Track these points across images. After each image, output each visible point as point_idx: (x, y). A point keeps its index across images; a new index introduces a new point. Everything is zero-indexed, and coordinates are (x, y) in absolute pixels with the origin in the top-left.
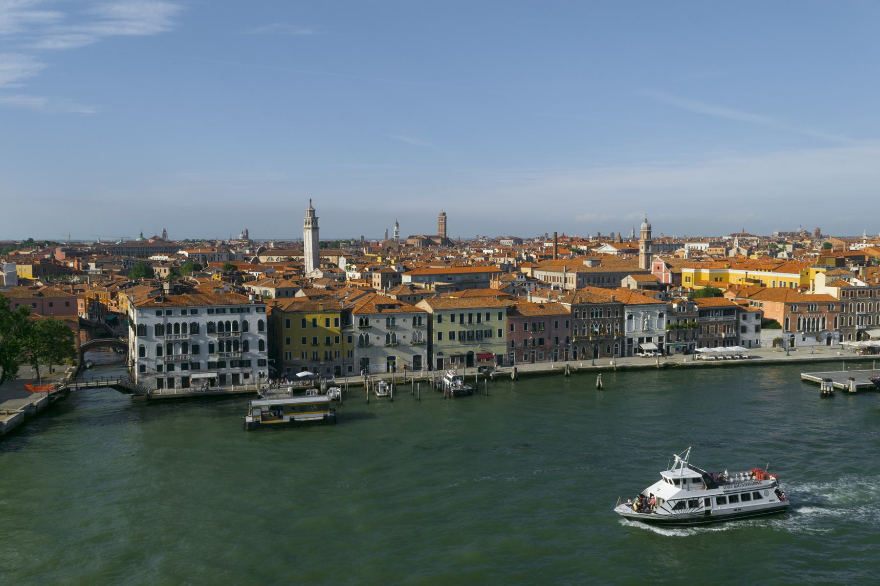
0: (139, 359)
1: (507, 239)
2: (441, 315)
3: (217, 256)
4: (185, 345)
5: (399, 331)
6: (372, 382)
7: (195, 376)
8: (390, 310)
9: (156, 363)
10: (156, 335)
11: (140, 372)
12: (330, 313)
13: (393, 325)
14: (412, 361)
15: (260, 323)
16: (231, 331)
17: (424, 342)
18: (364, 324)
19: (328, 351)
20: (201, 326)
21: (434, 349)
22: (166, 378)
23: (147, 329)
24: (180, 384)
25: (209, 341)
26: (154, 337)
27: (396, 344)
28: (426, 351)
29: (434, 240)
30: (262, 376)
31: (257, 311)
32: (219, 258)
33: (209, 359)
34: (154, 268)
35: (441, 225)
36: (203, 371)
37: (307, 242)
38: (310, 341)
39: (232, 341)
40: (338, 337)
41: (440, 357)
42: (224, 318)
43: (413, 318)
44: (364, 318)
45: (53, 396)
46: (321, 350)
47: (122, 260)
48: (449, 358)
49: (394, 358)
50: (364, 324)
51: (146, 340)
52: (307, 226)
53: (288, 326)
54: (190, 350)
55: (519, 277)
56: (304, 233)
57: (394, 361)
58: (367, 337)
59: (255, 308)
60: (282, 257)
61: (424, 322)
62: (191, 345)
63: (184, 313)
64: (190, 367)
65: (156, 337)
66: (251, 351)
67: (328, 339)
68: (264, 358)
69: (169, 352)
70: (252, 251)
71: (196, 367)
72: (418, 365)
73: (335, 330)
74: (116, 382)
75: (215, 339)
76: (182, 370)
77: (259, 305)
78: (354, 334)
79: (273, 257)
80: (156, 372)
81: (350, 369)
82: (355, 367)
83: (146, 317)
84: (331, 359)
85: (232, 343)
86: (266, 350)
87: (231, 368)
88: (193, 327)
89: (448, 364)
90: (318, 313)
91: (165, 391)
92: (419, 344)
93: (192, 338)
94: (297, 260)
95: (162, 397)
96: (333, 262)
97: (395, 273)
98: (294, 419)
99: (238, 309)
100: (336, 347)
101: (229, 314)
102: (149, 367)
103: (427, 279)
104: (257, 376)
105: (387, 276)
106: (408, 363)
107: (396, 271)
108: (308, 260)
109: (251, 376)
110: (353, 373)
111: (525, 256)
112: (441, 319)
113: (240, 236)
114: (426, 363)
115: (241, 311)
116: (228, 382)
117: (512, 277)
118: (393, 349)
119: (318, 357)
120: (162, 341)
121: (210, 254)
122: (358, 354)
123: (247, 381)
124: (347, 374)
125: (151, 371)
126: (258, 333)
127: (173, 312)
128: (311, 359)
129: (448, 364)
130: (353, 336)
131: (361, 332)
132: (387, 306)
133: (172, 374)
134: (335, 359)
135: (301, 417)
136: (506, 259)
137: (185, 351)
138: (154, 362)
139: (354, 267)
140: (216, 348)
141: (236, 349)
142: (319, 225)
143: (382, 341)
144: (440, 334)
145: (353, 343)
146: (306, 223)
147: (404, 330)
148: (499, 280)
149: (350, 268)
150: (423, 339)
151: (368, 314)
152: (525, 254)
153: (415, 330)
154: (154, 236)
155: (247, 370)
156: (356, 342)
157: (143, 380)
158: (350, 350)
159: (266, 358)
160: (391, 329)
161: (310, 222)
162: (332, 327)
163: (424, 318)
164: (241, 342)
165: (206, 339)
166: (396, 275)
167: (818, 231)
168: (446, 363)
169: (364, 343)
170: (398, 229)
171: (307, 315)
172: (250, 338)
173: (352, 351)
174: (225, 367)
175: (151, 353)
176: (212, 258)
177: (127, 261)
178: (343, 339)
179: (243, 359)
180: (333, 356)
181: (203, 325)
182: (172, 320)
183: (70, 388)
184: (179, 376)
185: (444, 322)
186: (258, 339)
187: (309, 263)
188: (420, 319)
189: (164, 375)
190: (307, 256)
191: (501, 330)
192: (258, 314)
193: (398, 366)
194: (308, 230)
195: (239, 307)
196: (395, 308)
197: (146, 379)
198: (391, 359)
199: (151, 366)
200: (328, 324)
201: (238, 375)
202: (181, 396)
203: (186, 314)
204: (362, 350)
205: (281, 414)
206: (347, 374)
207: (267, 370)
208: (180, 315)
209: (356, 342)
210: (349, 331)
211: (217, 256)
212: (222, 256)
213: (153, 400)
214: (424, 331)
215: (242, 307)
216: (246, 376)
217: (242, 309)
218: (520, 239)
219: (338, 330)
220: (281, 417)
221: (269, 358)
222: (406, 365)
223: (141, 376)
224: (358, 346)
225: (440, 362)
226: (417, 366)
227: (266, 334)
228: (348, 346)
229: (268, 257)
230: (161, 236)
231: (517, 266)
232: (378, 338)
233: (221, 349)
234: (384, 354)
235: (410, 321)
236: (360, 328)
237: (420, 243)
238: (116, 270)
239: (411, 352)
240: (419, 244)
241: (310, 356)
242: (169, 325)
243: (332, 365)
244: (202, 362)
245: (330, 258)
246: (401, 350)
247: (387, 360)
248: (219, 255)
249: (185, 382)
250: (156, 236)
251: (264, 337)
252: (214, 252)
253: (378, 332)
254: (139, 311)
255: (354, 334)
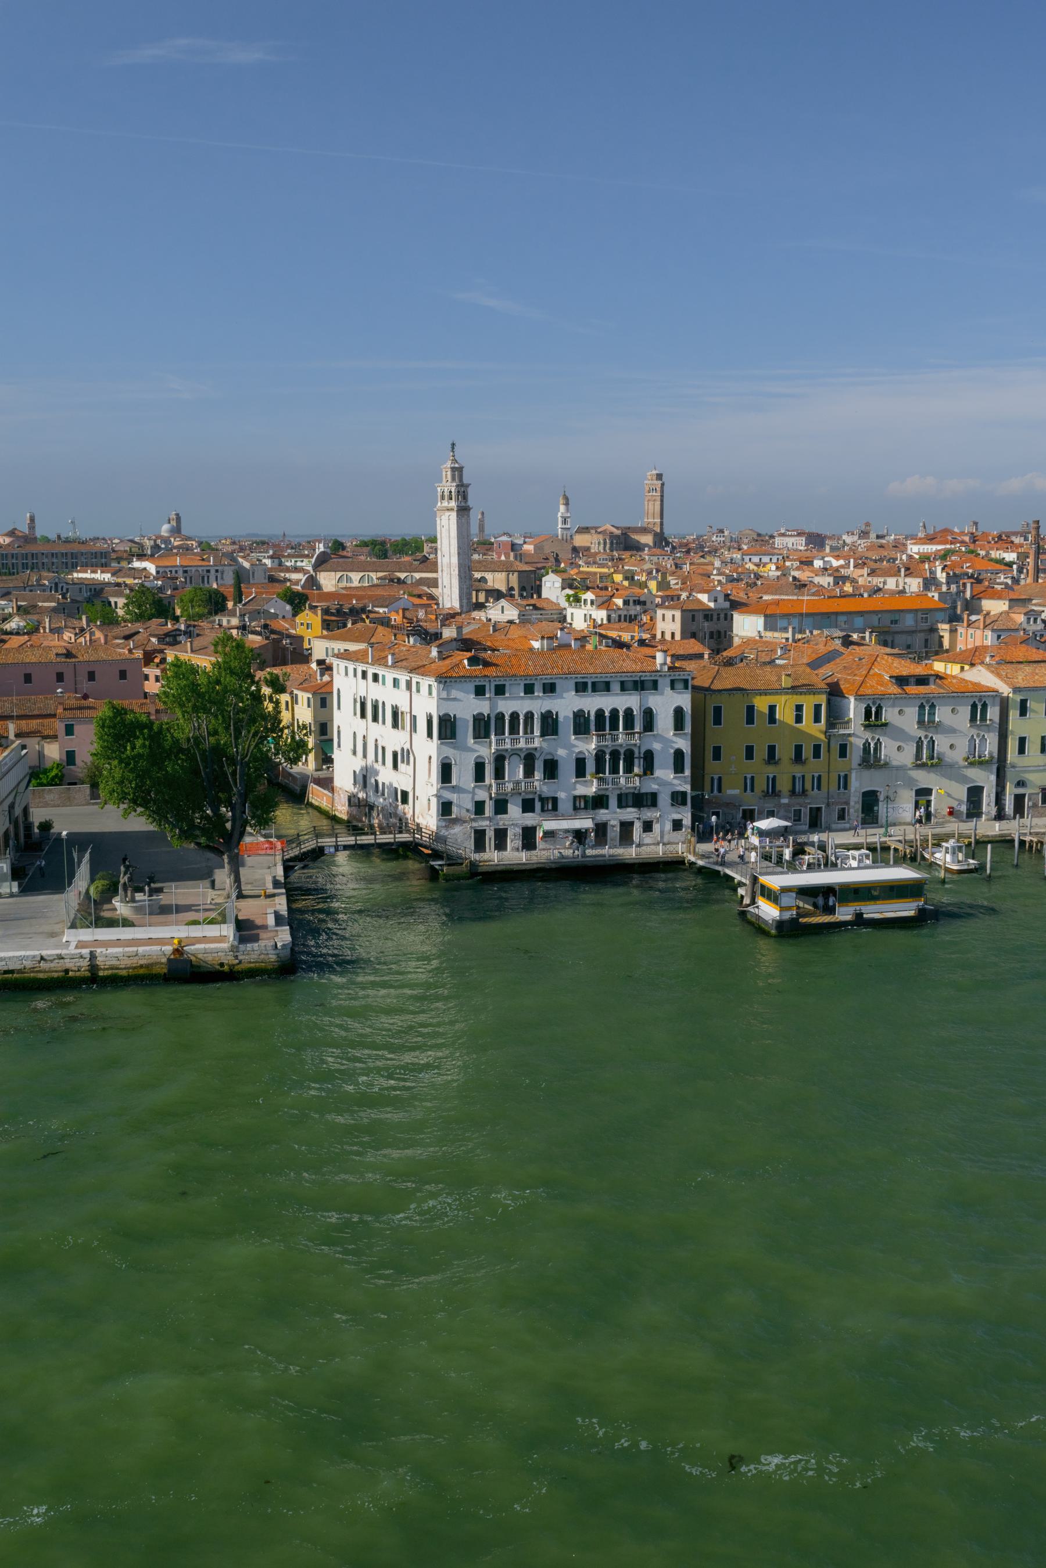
0: (442, 788)
1: (791, 536)
2: (1026, 700)
3: (213, 572)
4: (529, 760)
5: (942, 733)
6: (916, 840)
7: (550, 825)
8: (922, 689)
9: (473, 798)
10: (475, 738)
11: (443, 815)
12: (805, 694)
13: (932, 721)
14: (965, 800)
15: (679, 712)
16: (621, 729)
17: (992, 757)
18: (873, 718)
19: (798, 775)
20: (561, 719)
21: (1010, 773)
22: (492, 828)
23: (458, 723)
24: (519, 843)
25: (577, 750)
26: (471, 741)
27: (933, 763)
28: (993, 778)
29: (636, 537)
30: (677, 825)
31: (673, 688)
32: (217, 577)
33: (575, 789)
34: (112, 600)
35: (651, 503)
36: (563, 815)
37: (445, 542)
38: (761, 753)
39: (622, 751)
40: (820, 746)
41: (1020, 791)
42: (606, 702)
43: (972, 706)
44: (874, 703)
45: (291, 864)
46: (785, 772)
47: (46, 582)
48: (1038, 794)
49: (928, 792)
50: (873, 718)
51: (454, 748)
52: (445, 504)
53: (717, 721)
54: (539, 771)
55: (1029, 619)
56: (438, 519)
57: (928, 798)
58: (878, 743)
59: (668, 681)
60: (373, 575)
61: (993, 713)
62: (542, 758)
63: (529, 689)
64: (538, 805)
65: (475, 743)
66: (658, 773)
67: (798, 749)
68: (684, 790)
69: (499, 774)
70: (276, 561)
71: (550, 806)
72: (974, 808)
73: (814, 729)
74: (334, 839)
75: (590, 746)
76: (523, 812)
77: (677, 675)
78: (852, 739)
79: (352, 575)
80: (473, 816)
81: (842, 816)
82: (852, 811)
83: (455, 699)
84: (804, 791)
85: (622, 757)
86: (688, 772)
87: (618, 810)
88: (578, 718)
89: (1035, 805)
90: (781, 694)
91: (492, 857)
92: (981, 763)
93: (545, 745)
94: (409, 582)
95: (499, 868)
96: (497, 587)
97: (710, 610)
98: (862, 914)
99: (635, 682)
100: (814, 767)
101: (617, 694)
102: (459, 806)
103: (795, 622)
104: (669, 826)
105: (693, 616)
106: (957, 803)
107: (712, 605)
108: (446, 582)
109: (656, 827)
110: (848, 823)
111: (944, 574)
112: (1026, 707)
113: (165, 530)
114: (993, 804)
115: (640, 685)
116: (612, 840)
117: (1012, 619)
118: (929, 772)
119: (778, 788)
120: (487, 750)
121: (200, 569)
122: (859, 783)
123: (648, 838)
124: (834, 826)
125: (464, 815)
126: (675, 735)
127: (507, 688)
128: (763, 791)
129: (1035, 805)
130: (851, 743)
131: (868, 735)
132: (912, 680)
133: (502, 820)
134: (810, 793)
135: (873, 911)
136: (901, 580)
137: (529, 772)
138: (470, 796)
139: (589, 596)
140: (590, 766)
141: (629, 769)
142: (470, 503)
143: (907, 757)
144: (1022, 741)
145: (850, 759)
146: (443, 498)
147: (952, 731)
148: (985, 627)
149: (577, 600)
150: (989, 753)
151: (883, 696)
152: (943, 569)
153: (974, 732)
154: (10, 529)
155: (649, 814)
156: (855, 756)
157: (446, 834)
158: (842, 774)
159: (687, 788)
160: (927, 729)
161: (453, 494)
162: (807, 724)
163: (994, 705)
164: (640, 753)
165: (569, 747)
166: (712, 615)
167: (114, 556)
168: (1031, 804)
169: (870, 759)
170: (567, 510)
171: (758, 697)
172: (656, 746)
173: (846, 776)
174: (607, 808)
175: (463, 775)
176: (203, 578)
177: (56, 584)
178: (829, 751)
179: (643, 791)
180: (808, 786)
181: (566, 718)
182: (506, 706)
183: (323, 847)
184: (516, 825)
185: (1033, 715)
186: (672, 747)
187: (448, 586)
188: (985, 706)
189: (488, 823)
190: (445, 574)
191: (1025, 738)
192: (675, 695)
193: (936, 810)
194: (447, 513)
195: (638, 679)
196: (928, 684)
197: (452, 831)
198: (924, 793)
199: (462, 805)
200: (799, 719)
201: (632, 824)
202: (535, 866)
203: (533, 693)
204: (867, 774)
205: (831, 903)
206: (834, 826)
207: (690, 815)
208: (522, 694)
209: (855, 756)
210: (842, 732)
211: (213, 572)
212: (222, 573)
213: (483, 874)
214: (992, 734)
215: (642, 679)
216: (648, 827)
217: (642, 682)
218: (819, 535)
219: (821, 731)
220: (831, 910)
221: (692, 790)
222: (953, 808)
223: (444, 824)
224: (860, 765)
225: (1019, 800)
226: (974, 810)
227: (689, 737)
228: (839, 765)
229: (339, 574)
230: (26, 530)
231: (973, 597)
232: (899, 748)
233: (599, 769)
234: (910, 782)
235: (965, 711)
236: (866, 727)
237: (605, 543)
238: (46, 604)
239: (964, 779)
240: (602, 546)
241: (761, 785)
242: (500, 717)
243: (806, 807)
244: (562, 795)
245: (489, 576)
246: (943, 776)
247: (916, 795)
248: (217, 571)
249: (528, 838)
250: (15, 529)
251: (684, 744)
252: (207, 564)
253: (899, 734)
254: (442, 686)
255: (852, 739)
